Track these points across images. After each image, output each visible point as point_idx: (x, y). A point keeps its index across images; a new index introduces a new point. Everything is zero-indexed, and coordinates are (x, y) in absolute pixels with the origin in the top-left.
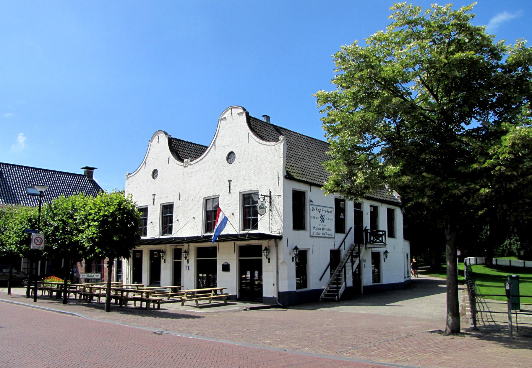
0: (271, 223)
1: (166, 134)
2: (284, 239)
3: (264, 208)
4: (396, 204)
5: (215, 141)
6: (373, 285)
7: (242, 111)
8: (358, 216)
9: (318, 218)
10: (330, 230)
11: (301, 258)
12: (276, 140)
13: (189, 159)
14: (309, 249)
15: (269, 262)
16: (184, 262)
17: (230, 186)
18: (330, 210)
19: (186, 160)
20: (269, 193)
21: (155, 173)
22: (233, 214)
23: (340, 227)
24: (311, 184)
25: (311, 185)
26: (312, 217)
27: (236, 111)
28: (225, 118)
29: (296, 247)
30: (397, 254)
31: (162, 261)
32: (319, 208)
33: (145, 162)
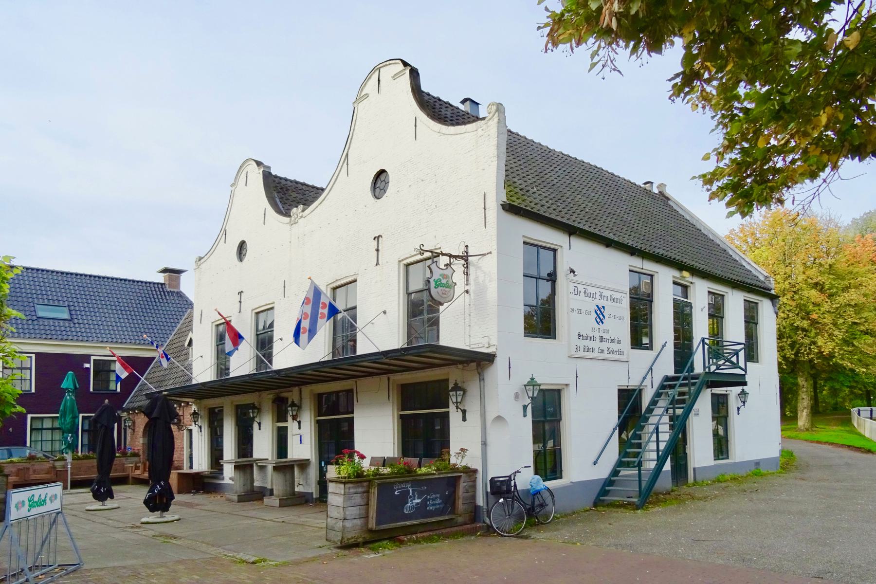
1: (259, 164)
2: (500, 364)
3: (451, 286)
5: (347, 155)
6: (716, 466)
7: (401, 66)
8: (682, 316)
9: (588, 313)
10: (619, 342)
11: (547, 411)
15: (464, 419)
16: (292, 426)
17: (377, 250)
18: (617, 295)
19: (295, 210)
20: (464, 249)
22: (385, 312)
23: (640, 331)
24: (571, 231)
28: (367, 95)
29: (532, 379)
31: (256, 426)
32: (591, 290)
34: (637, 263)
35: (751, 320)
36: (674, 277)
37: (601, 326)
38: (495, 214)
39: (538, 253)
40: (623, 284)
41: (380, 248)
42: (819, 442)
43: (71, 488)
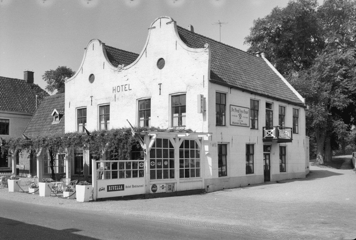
0: (197, 122)
4: (300, 105)
5: (146, 49)
9: (237, 116)
12: (202, 46)
13: (123, 65)
14: (229, 143)
17: (160, 89)
21: (92, 78)
25: (231, 88)
26: (230, 116)
27: (164, 21)
28: (154, 27)
30: (298, 147)
33: (82, 68)
34: (253, 97)
35: (296, 118)
36: (266, 101)
37: (241, 120)
38: (208, 84)
39: (220, 95)
40: (248, 105)
41: (161, 88)
42: (133, 186)
43: (196, 177)
